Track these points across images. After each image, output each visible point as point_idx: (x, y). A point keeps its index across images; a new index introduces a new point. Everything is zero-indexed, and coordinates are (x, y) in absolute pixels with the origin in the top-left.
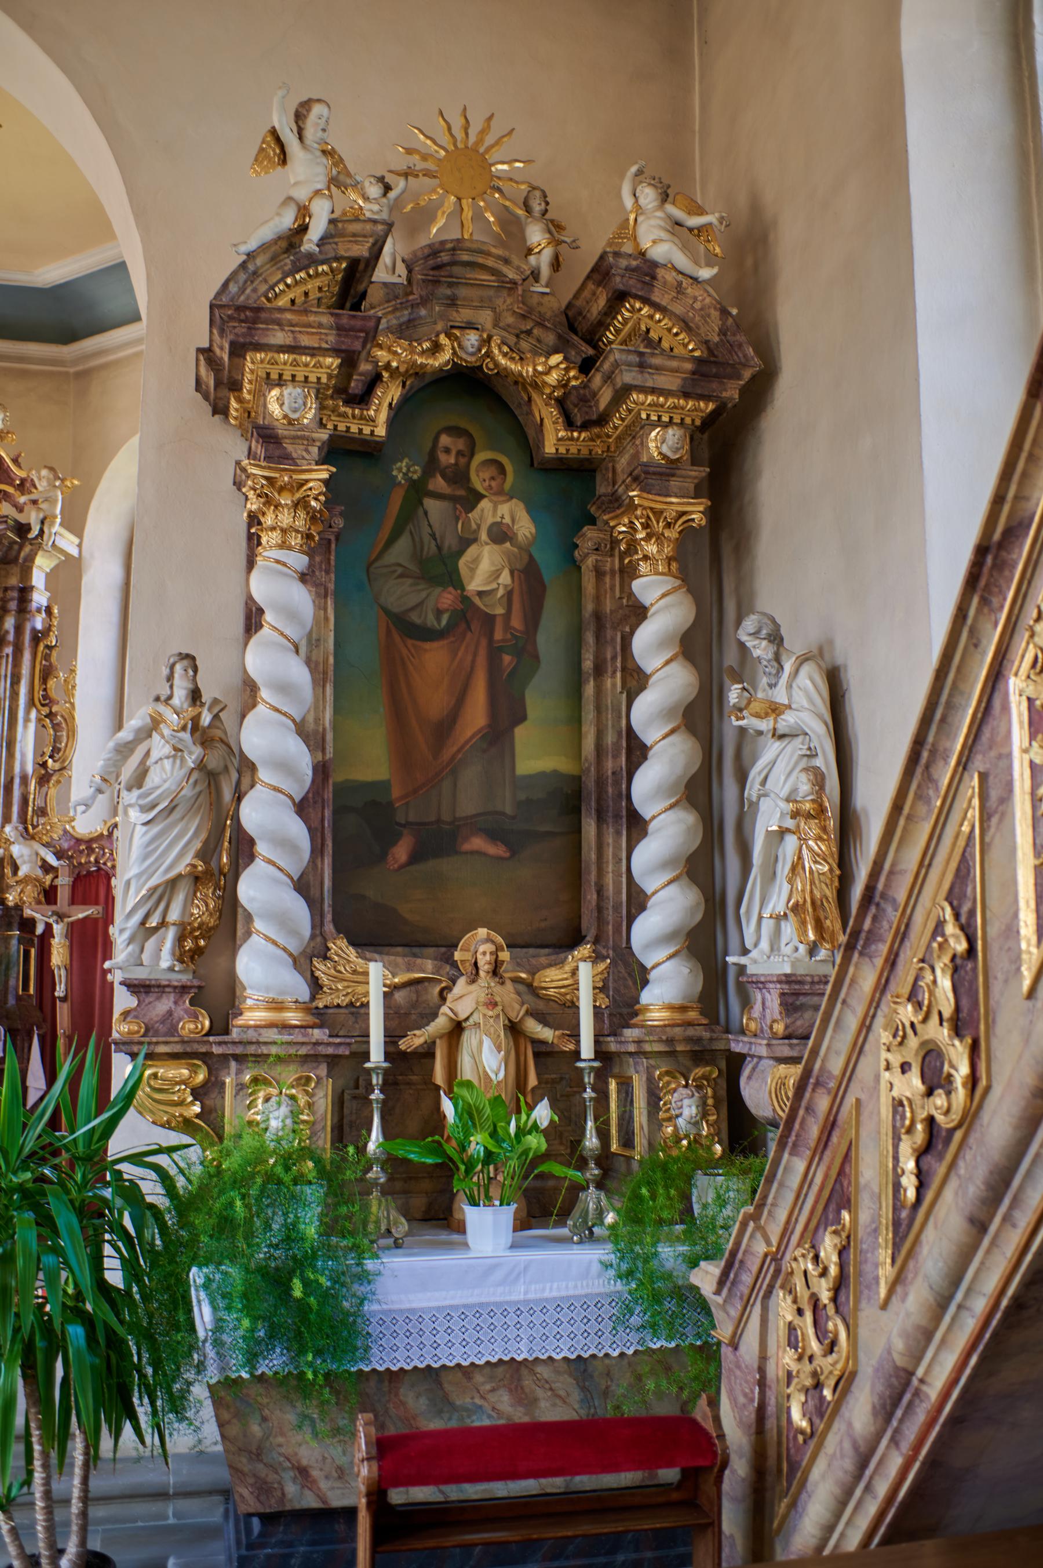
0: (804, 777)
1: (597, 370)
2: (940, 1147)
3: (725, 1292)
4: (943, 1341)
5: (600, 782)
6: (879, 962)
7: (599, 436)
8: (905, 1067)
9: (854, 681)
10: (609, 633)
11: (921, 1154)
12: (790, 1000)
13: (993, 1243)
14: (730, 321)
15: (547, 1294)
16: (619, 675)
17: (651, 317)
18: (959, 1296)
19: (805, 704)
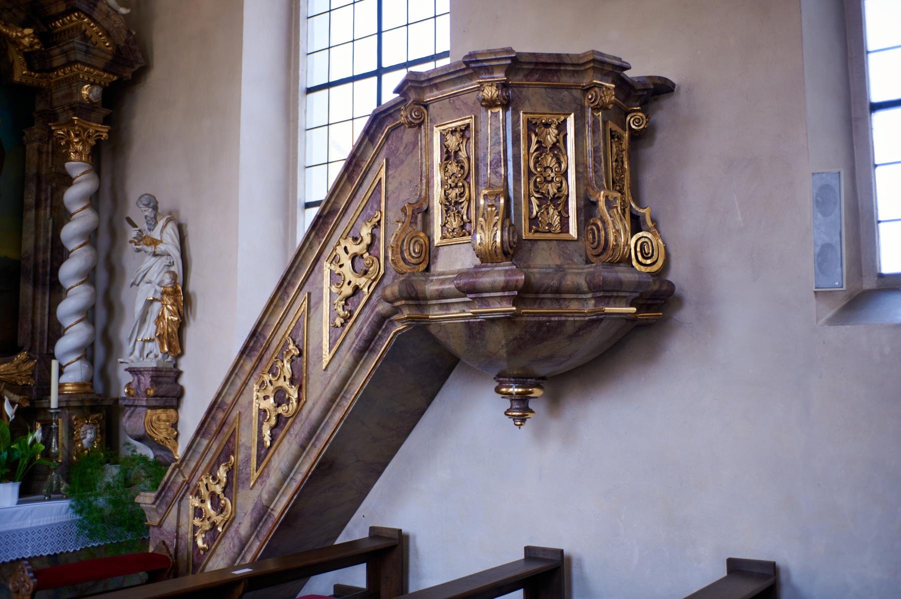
0: (167, 276)
1: (59, 47)
3: (158, 502)
4: (283, 493)
5: (36, 266)
6: (254, 359)
7: (45, 77)
8: (266, 398)
9: (191, 231)
10: (44, 186)
11: (272, 429)
12: (155, 379)
13: (307, 454)
14: (131, 37)
15: (41, 524)
16: (48, 209)
17: (89, 24)
18: (292, 475)
19: (170, 241)
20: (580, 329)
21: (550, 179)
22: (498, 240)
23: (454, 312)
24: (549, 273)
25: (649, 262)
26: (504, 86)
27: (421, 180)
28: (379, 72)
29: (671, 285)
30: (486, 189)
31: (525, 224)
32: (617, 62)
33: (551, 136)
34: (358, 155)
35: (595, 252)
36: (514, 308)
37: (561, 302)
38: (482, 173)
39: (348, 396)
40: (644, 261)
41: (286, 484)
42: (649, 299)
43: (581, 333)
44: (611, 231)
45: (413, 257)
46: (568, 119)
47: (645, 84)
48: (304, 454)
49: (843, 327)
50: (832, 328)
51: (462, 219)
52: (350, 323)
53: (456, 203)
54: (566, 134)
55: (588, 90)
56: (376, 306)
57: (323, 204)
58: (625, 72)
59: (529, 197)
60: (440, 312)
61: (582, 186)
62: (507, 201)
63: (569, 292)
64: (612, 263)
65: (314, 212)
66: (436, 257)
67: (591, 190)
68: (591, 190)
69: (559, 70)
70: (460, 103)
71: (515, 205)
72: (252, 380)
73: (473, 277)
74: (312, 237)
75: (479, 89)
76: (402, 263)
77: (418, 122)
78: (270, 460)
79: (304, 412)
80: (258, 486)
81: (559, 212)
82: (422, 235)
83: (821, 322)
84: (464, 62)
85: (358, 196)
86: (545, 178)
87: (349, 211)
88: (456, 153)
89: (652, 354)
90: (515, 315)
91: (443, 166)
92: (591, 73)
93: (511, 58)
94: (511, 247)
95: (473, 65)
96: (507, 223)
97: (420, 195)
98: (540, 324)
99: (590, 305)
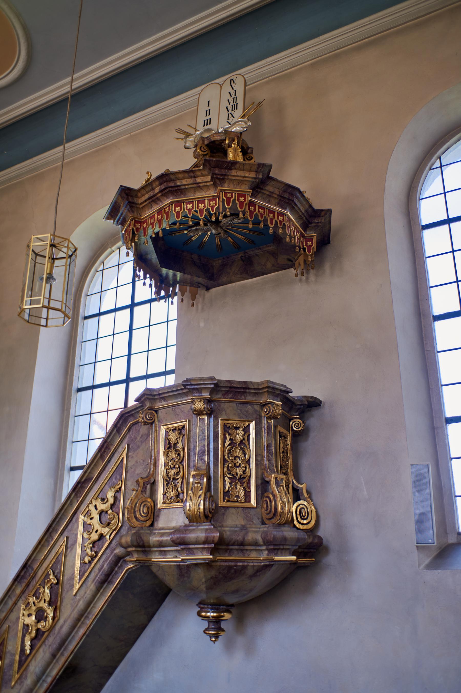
2: (40, 637)
6: (24, 585)
8: (29, 615)
11: (32, 640)
18: (44, 678)
20: (258, 571)
21: (238, 464)
22: (202, 507)
23: (169, 558)
24: (236, 531)
25: (305, 522)
26: (209, 401)
27: (151, 461)
28: (128, 381)
29: (320, 538)
30: (195, 471)
31: (220, 495)
32: (283, 388)
33: (239, 436)
34: (109, 440)
35: (268, 517)
36: (211, 557)
37: (245, 551)
38: (192, 459)
39: (90, 616)
40: (302, 521)
41: (39, 685)
42: (306, 548)
43: (258, 574)
44: (279, 502)
45: (142, 516)
46: (251, 425)
47: (302, 401)
48: (55, 661)
49: (436, 571)
50: (429, 571)
51: (177, 490)
52: (95, 561)
53: (174, 479)
54: (250, 434)
55: (264, 405)
56: (114, 549)
57: (85, 468)
58: (289, 394)
59: (224, 477)
60: (160, 557)
61: (259, 470)
62: (209, 479)
63: (250, 545)
64: (279, 525)
65: (77, 475)
66: (158, 516)
67: (266, 473)
68: (266, 473)
69: (246, 392)
70: (179, 411)
71: (214, 482)
72: (21, 601)
73: (183, 534)
74: (72, 497)
75: (193, 402)
76: (134, 520)
77: (150, 421)
78: (28, 665)
79: (57, 628)
80: (18, 686)
81: (244, 488)
82: (149, 500)
83: (422, 566)
84: (183, 385)
85: (107, 469)
86: (235, 464)
87: (99, 479)
88: (175, 444)
89: (308, 589)
90: (212, 561)
91: (166, 453)
92: (266, 395)
93: (214, 384)
94: (210, 512)
95: (189, 387)
96: (208, 495)
97: (149, 472)
98: (230, 567)
99: (264, 555)
